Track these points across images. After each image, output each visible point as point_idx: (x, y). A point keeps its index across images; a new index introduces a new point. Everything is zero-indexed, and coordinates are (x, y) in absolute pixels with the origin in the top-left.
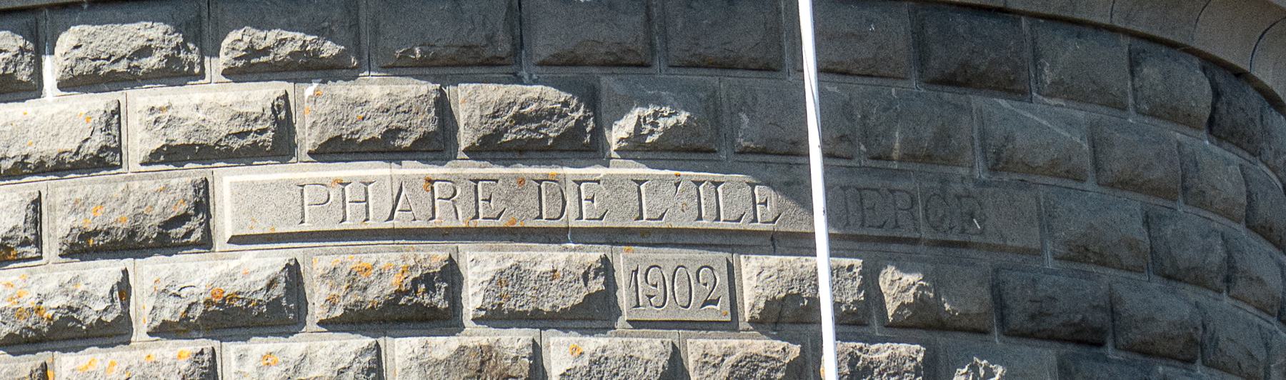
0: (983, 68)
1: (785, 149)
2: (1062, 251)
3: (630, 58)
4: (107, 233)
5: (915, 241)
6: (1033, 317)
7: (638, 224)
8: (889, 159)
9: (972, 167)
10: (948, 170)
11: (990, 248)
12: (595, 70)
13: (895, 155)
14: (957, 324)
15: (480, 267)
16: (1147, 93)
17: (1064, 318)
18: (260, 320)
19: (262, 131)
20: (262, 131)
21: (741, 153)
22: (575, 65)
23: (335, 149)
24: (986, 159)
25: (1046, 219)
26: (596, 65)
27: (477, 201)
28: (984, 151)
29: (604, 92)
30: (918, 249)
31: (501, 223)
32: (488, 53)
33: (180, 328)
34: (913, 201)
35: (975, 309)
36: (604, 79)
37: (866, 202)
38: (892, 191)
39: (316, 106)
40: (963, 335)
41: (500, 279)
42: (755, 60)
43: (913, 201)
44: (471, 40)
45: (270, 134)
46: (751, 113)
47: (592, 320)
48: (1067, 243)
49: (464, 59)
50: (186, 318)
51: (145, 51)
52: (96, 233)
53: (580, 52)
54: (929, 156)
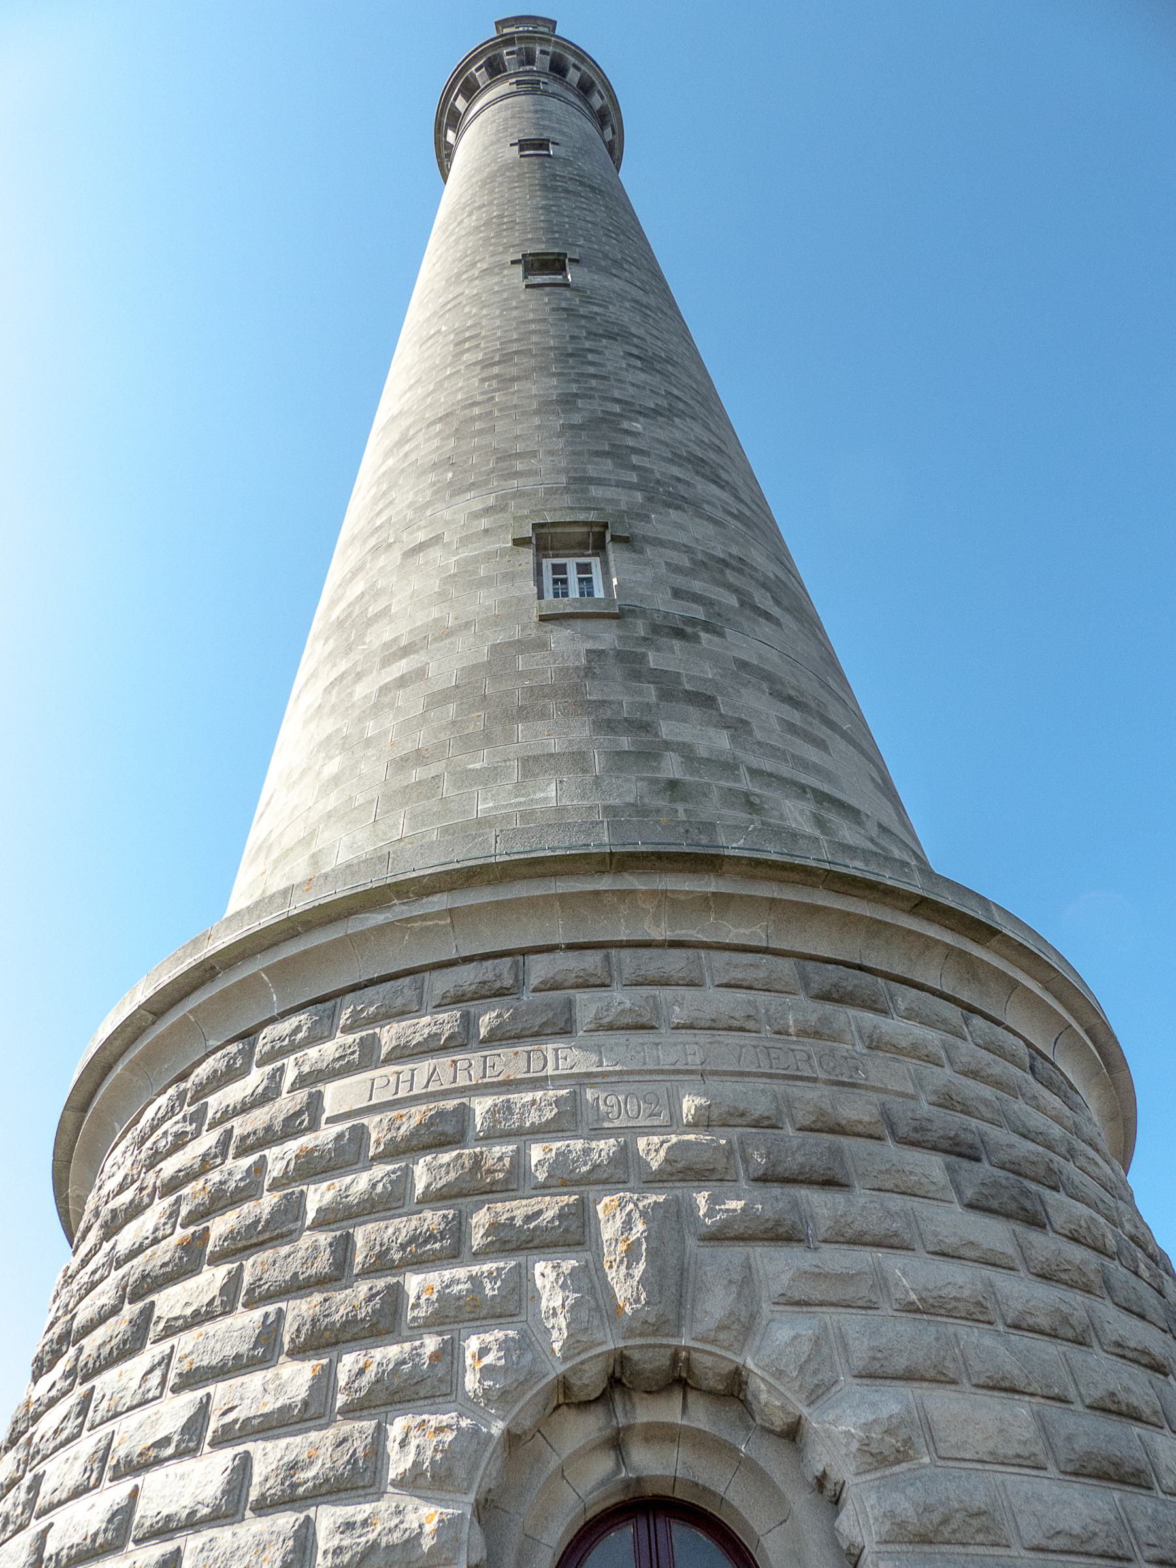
0: (850, 988)
1: (707, 1025)
2: (934, 1098)
3: (592, 981)
4: (255, 1133)
5: (815, 1080)
6: (916, 1130)
7: (600, 1069)
8: (789, 1035)
9: (853, 1045)
10: (835, 1044)
11: (874, 1089)
12: (572, 991)
13: (792, 1030)
14: (855, 1129)
15: (481, 1106)
16: (979, 1033)
17: (941, 1133)
18: (332, 1163)
19: (353, 1053)
20: (353, 1053)
21: (677, 1028)
22: (557, 989)
23: (402, 1054)
24: (863, 1042)
25: (919, 1081)
26: (571, 987)
27: (485, 1068)
28: (861, 1038)
29: (578, 1002)
30: (818, 1085)
31: (500, 1078)
32: (498, 985)
33: (284, 1181)
34: (809, 1057)
35: (866, 1119)
36: (577, 996)
37: (773, 1055)
38: (793, 1050)
39: (388, 1035)
40: (863, 1140)
41: (492, 1112)
42: (683, 978)
43: (809, 1057)
44: (485, 978)
45: (356, 1055)
46: (681, 1005)
47: (563, 1131)
48: (935, 1092)
49: (483, 992)
50: (286, 1172)
51: (298, 1029)
52: (249, 1135)
53: (559, 978)
54: (816, 1033)
